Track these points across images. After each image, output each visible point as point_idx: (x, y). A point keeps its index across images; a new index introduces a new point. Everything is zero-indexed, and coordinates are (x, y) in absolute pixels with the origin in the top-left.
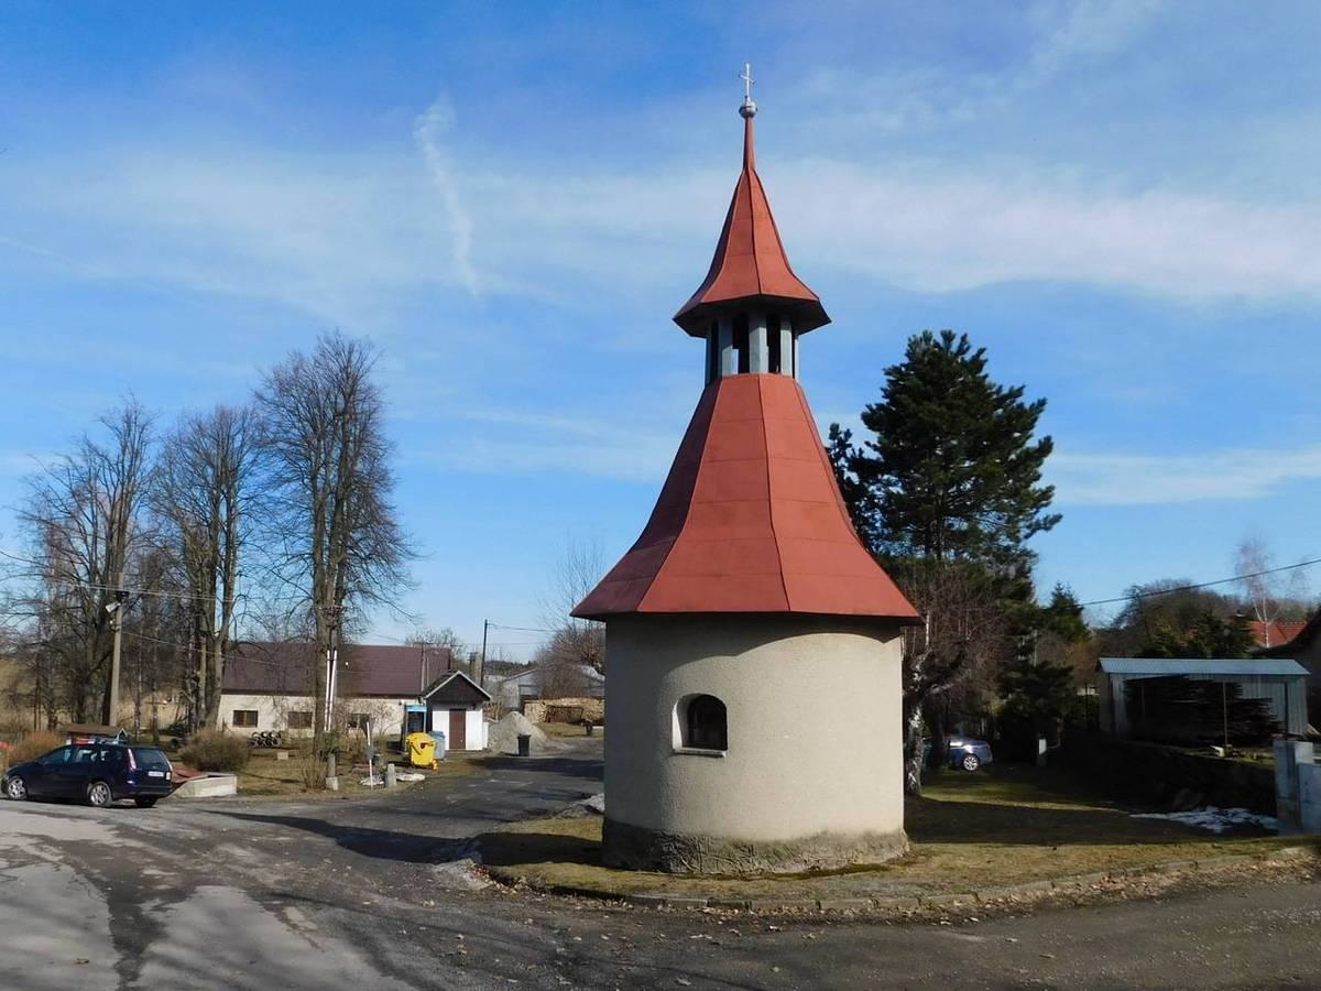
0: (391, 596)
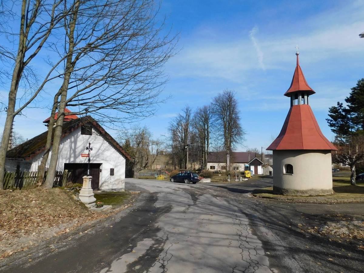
0: (241, 142)
